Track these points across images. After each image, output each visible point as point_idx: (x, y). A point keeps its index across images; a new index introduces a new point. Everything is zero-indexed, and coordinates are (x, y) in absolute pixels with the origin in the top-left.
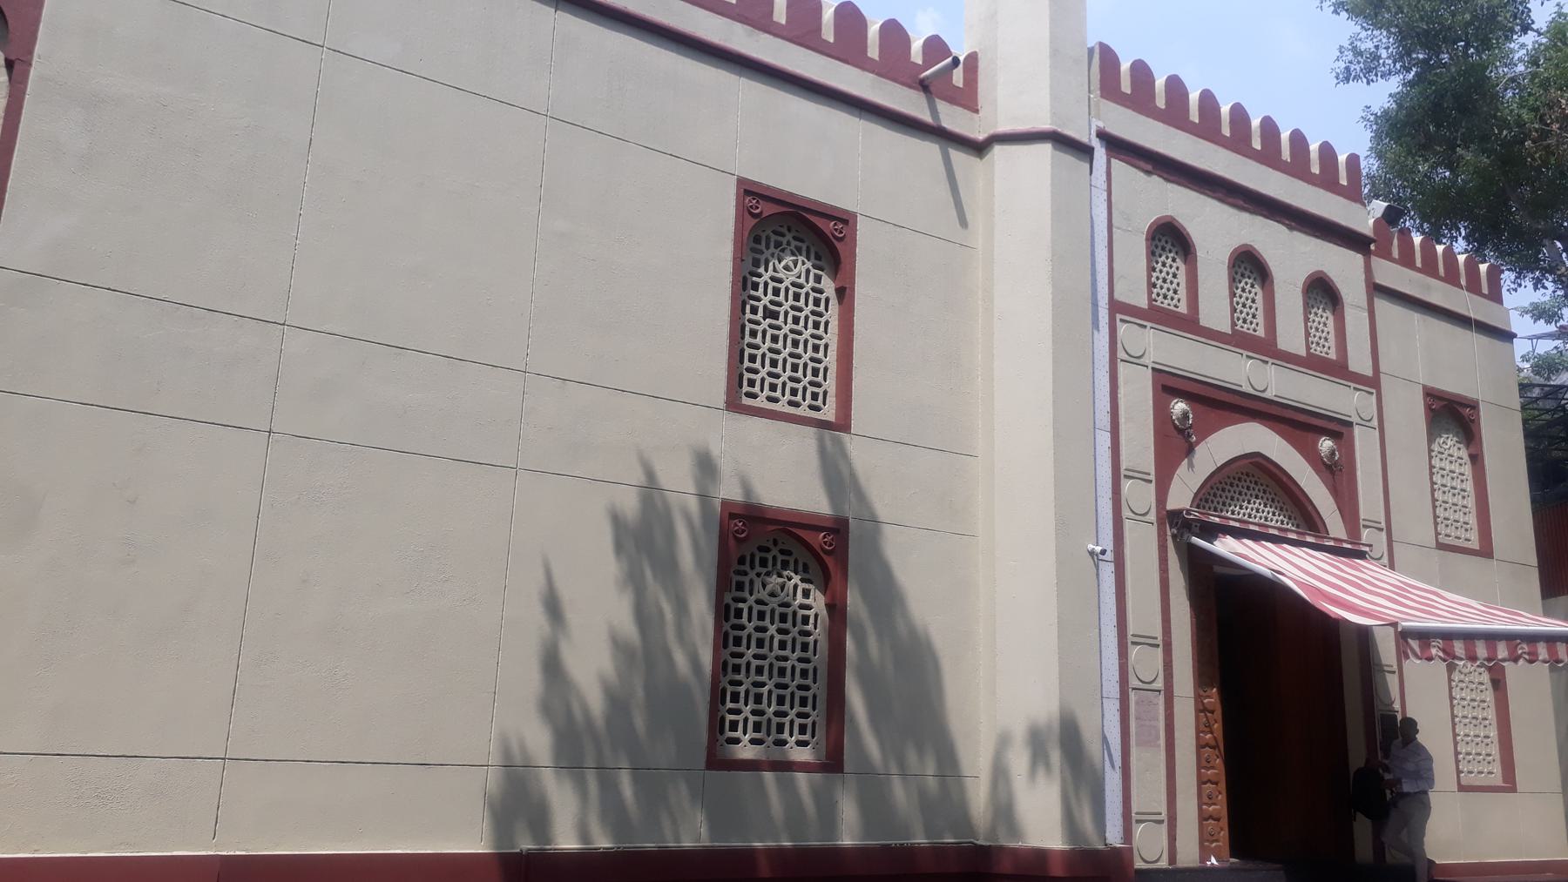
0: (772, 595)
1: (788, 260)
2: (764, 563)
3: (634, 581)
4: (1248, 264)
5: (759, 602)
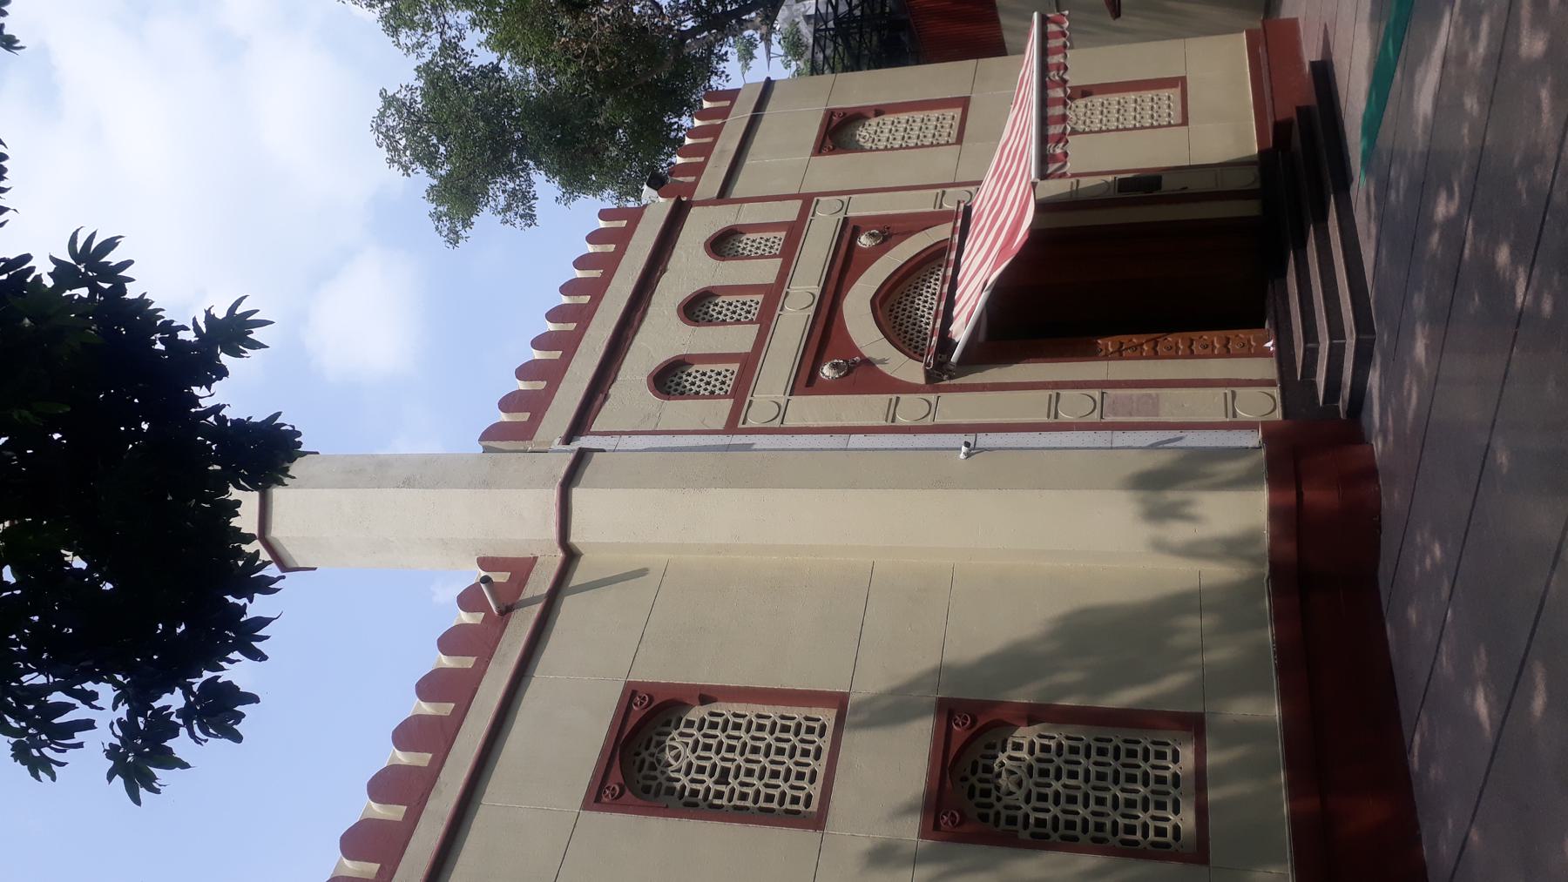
0: (1019, 784)
1: (669, 756)
4: (695, 309)
5: (1028, 800)
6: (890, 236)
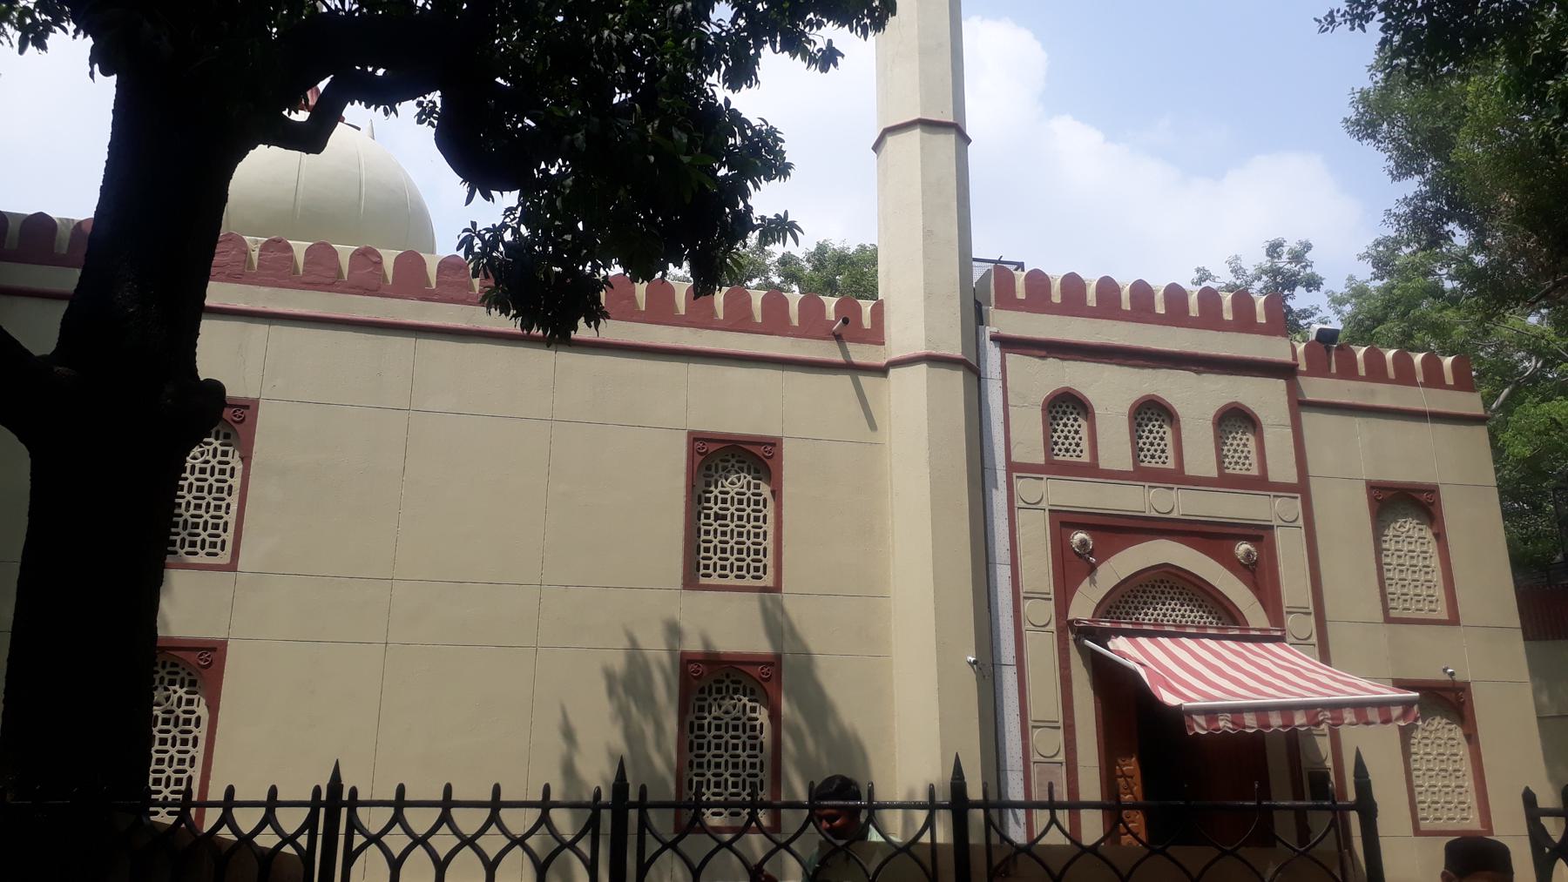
0: (727, 712)
1: (733, 477)
2: (719, 691)
3: (623, 714)
4: (1151, 411)
6: (1253, 572)
